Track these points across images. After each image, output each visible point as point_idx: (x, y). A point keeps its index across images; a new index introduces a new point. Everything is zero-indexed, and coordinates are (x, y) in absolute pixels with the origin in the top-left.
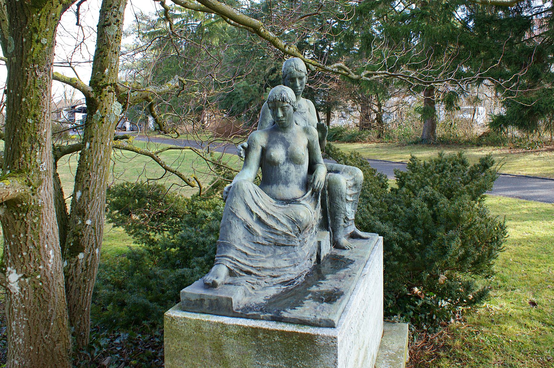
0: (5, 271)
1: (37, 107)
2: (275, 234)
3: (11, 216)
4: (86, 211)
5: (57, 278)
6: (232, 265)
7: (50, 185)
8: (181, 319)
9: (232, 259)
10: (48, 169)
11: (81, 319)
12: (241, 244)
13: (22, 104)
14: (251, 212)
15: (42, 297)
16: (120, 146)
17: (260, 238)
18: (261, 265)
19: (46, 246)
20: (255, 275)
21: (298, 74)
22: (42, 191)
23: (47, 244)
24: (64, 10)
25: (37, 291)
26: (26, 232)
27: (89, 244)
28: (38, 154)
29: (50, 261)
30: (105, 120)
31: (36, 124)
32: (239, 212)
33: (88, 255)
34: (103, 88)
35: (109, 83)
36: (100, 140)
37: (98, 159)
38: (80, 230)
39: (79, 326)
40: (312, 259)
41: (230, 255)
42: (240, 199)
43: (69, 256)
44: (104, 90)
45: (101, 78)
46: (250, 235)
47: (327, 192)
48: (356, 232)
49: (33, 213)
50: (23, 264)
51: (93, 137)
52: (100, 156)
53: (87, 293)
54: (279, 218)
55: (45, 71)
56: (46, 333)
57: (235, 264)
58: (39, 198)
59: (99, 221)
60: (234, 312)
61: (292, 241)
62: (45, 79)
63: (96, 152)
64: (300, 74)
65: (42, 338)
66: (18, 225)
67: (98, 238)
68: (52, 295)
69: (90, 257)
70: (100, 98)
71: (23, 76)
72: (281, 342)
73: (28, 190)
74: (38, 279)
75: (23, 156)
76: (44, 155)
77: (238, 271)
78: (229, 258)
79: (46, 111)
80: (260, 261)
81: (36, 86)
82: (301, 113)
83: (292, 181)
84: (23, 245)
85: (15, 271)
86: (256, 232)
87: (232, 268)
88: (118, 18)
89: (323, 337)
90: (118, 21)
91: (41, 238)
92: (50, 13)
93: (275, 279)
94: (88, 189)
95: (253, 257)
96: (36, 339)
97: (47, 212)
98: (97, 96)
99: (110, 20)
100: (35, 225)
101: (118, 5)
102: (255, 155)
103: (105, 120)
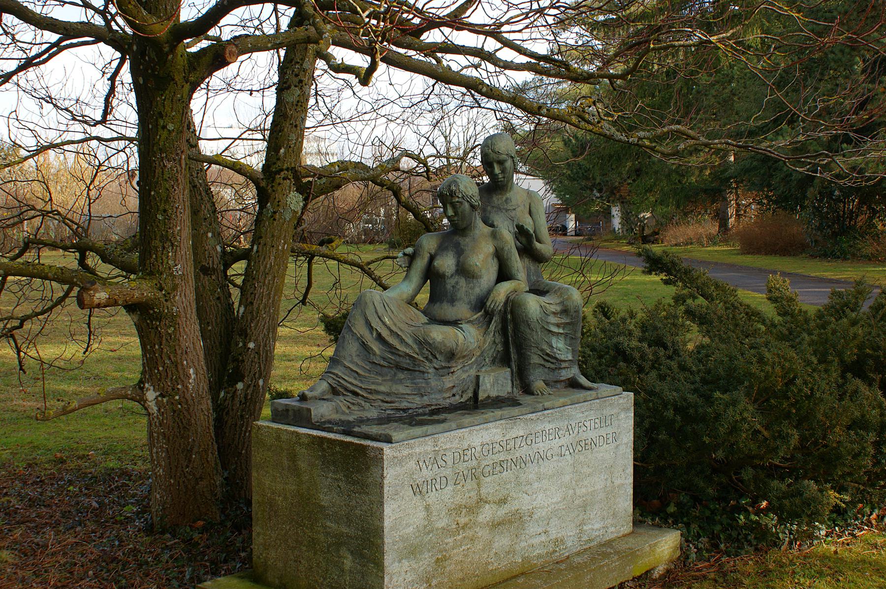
0: (143, 388)
1: (167, 201)
2: (396, 354)
3: (145, 324)
4: (249, 331)
5: (200, 403)
7: (188, 292)
8: (265, 427)
9: (337, 375)
10: (185, 273)
11: (236, 463)
12: (352, 362)
13: (151, 198)
14: (371, 328)
17: (378, 358)
18: (373, 387)
19: (185, 362)
20: (363, 396)
22: (177, 298)
24: (193, 90)
25: (176, 415)
28: (170, 254)
30: (277, 216)
32: (356, 326)
33: (249, 386)
35: (285, 167)
37: (266, 267)
38: (240, 354)
39: (234, 471)
40: (464, 396)
41: (336, 371)
42: (360, 311)
43: (226, 385)
44: (278, 176)
45: (275, 160)
46: (366, 353)
47: (509, 316)
48: (576, 379)
49: (167, 322)
50: (160, 380)
51: (261, 237)
53: (245, 432)
54: (404, 337)
55: (175, 160)
56: (187, 466)
60: (313, 424)
61: (419, 366)
63: (265, 258)
65: (183, 471)
66: (153, 335)
67: (262, 366)
68: (193, 422)
69: (251, 388)
70: (272, 187)
71: (151, 166)
72: (340, 452)
73: (160, 295)
74: (176, 400)
76: (179, 256)
78: (334, 374)
80: (373, 383)
81: (165, 177)
82: (507, 210)
83: (460, 299)
84: (159, 358)
85: (152, 388)
86: (372, 349)
87: (335, 386)
88: (301, 77)
89: (373, 448)
90: (301, 81)
91: (179, 352)
92: (174, 95)
93: (386, 404)
94: (252, 303)
95: (365, 377)
96: (176, 471)
98: (268, 185)
99: (290, 81)
100: (171, 336)
101: (302, 59)
102: (420, 264)
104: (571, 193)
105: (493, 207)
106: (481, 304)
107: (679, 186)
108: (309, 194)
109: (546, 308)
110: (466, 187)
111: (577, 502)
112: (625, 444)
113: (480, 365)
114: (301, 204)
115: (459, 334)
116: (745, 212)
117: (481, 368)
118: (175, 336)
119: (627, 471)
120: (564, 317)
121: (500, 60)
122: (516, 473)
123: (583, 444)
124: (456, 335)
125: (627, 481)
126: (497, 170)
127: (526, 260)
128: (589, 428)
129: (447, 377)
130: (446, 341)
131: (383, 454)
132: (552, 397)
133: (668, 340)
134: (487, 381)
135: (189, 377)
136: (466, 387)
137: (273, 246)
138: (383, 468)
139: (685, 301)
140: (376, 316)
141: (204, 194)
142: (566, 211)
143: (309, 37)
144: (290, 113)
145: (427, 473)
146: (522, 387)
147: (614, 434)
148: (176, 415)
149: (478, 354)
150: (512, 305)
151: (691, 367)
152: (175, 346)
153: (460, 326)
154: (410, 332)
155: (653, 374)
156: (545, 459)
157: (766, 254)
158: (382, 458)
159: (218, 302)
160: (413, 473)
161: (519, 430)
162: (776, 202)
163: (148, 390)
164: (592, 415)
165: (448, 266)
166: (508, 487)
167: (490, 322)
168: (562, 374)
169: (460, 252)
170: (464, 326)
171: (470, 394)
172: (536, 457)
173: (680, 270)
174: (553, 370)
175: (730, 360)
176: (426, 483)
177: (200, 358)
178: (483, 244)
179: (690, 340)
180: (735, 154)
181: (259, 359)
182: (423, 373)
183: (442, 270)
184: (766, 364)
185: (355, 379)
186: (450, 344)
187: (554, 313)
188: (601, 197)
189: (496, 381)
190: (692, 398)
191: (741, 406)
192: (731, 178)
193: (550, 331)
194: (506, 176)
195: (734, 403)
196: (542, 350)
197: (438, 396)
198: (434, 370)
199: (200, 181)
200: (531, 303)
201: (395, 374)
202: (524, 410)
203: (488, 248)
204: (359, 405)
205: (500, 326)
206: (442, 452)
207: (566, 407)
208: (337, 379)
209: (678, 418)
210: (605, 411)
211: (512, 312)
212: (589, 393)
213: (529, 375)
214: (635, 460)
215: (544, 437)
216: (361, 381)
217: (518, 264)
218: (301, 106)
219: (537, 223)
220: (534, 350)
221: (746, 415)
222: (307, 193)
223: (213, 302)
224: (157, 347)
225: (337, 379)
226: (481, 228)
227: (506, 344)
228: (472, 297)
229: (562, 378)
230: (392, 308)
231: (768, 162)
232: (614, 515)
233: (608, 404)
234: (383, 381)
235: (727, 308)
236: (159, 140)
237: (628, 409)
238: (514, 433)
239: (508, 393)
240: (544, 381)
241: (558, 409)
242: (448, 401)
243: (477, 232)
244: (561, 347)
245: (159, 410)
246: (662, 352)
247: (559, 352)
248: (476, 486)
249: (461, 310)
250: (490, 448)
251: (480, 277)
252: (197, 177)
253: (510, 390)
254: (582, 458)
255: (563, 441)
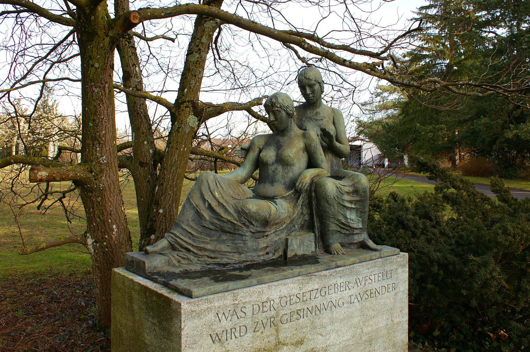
1: (95, 114)
4: (160, 202)
6: (173, 240)
9: (175, 235)
10: (109, 162)
12: (188, 225)
14: (204, 200)
15: (109, 260)
16: (210, 155)
18: (202, 245)
19: (110, 221)
20: (193, 252)
21: (306, 82)
22: (103, 178)
23: (111, 219)
25: (105, 255)
26: (93, 208)
27: (159, 228)
28: (98, 149)
29: (114, 233)
30: (180, 130)
31: (95, 127)
34: (181, 104)
35: (187, 100)
36: (175, 146)
37: (172, 161)
38: (154, 217)
40: (276, 254)
41: (175, 232)
44: (182, 105)
46: (199, 219)
47: (313, 194)
48: (365, 242)
50: (94, 232)
52: (174, 159)
54: (227, 207)
55: (100, 87)
57: (176, 240)
58: (101, 183)
59: (170, 211)
61: (238, 230)
62: (100, 93)
63: (172, 155)
64: (309, 82)
70: (178, 112)
72: (156, 301)
73: (90, 175)
74: (105, 245)
75: (88, 150)
77: (177, 246)
79: (103, 118)
80: (203, 242)
81: (94, 98)
82: (316, 120)
83: (278, 181)
84: (93, 217)
85: (90, 236)
87: (173, 243)
90: (200, 49)
91: (106, 214)
94: (162, 184)
95: (197, 237)
97: (109, 194)
99: (193, 49)
100: (99, 203)
103: (181, 130)
104: (386, 149)
105: (307, 118)
106: (292, 185)
107: (434, 146)
108: (201, 117)
109: (341, 188)
110: (283, 100)
111: (364, 338)
112: (402, 291)
113: (290, 230)
114: (197, 123)
115: (272, 206)
116: (463, 158)
117: (291, 232)
118: (103, 203)
119: (404, 312)
120: (355, 196)
121: (325, 42)
122: (312, 319)
123: (369, 293)
124: (270, 207)
125: (404, 319)
126: (308, 91)
127: (330, 155)
128: (373, 281)
129: (262, 239)
130: (260, 212)
131: (181, 308)
132: (345, 257)
133: (432, 214)
134: (294, 243)
135: (113, 230)
136: (278, 247)
137: (177, 149)
138: (181, 320)
139: (442, 190)
140: (208, 191)
141: (143, 118)
142: (384, 157)
143: (188, 9)
144: (192, 68)
145: (226, 324)
146: (324, 248)
147: (394, 285)
148: (105, 255)
149: (288, 222)
150: (315, 186)
151: (449, 234)
152: (102, 210)
153: (275, 200)
154: (233, 203)
155: (423, 237)
156: (337, 307)
157: (474, 176)
158: (180, 312)
159: (148, 184)
160: (212, 324)
161: (314, 284)
162: (477, 153)
163: (88, 238)
164: (376, 270)
165: (270, 156)
166: (304, 331)
167: (298, 198)
168: (355, 238)
169: (279, 147)
170: (278, 201)
171: (281, 253)
172: (330, 305)
173: (438, 170)
174: (348, 235)
175: (478, 230)
176: (225, 332)
177: (121, 218)
178: (296, 141)
179: (445, 215)
180: (458, 131)
181: (166, 220)
182: (242, 235)
183: (265, 159)
184: (509, 235)
185: (190, 238)
186: (264, 213)
187: (348, 193)
188: (399, 151)
189: (302, 243)
190: (451, 257)
191: (490, 267)
192: (457, 142)
193: (345, 206)
194: (315, 95)
195: (485, 264)
196: (338, 220)
197: (253, 254)
198: (251, 234)
199: (142, 111)
200: (329, 184)
201: (220, 236)
202: (319, 267)
203: (300, 144)
204: (188, 259)
205: (307, 201)
206: (242, 305)
207: (355, 265)
208: (175, 238)
209: (441, 272)
210: (386, 267)
211: (315, 191)
212: (374, 253)
213: (329, 239)
214: (409, 301)
215: (336, 289)
216: (194, 240)
217: (321, 155)
218: (199, 64)
219: (338, 130)
220: (332, 220)
221: (494, 274)
222: (201, 116)
223: (145, 184)
224: (91, 210)
225: (175, 238)
226: (296, 130)
227: (311, 215)
228: (287, 180)
229: (355, 241)
230: (223, 185)
231: (474, 133)
232: (394, 345)
233: (388, 261)
234: (210, 240)
235: (469, 196)
236: (90, 73)
237: (404, 266)
238: (309, 287)
239: (312, 252)
240: (340, 243)
241: (348, 267)
242: (262, 258)
243: (292, 133)
244: (353, 218)
245: (95, 251)
246: (428, 223)
247: (352, 222)
248: (275, 332)
249: (278, 189)
250: (288, 300)
251: (293, 165)
252: (140, 108)
253: (313, 249)
254: (368, 304)
255: (352, 292)
